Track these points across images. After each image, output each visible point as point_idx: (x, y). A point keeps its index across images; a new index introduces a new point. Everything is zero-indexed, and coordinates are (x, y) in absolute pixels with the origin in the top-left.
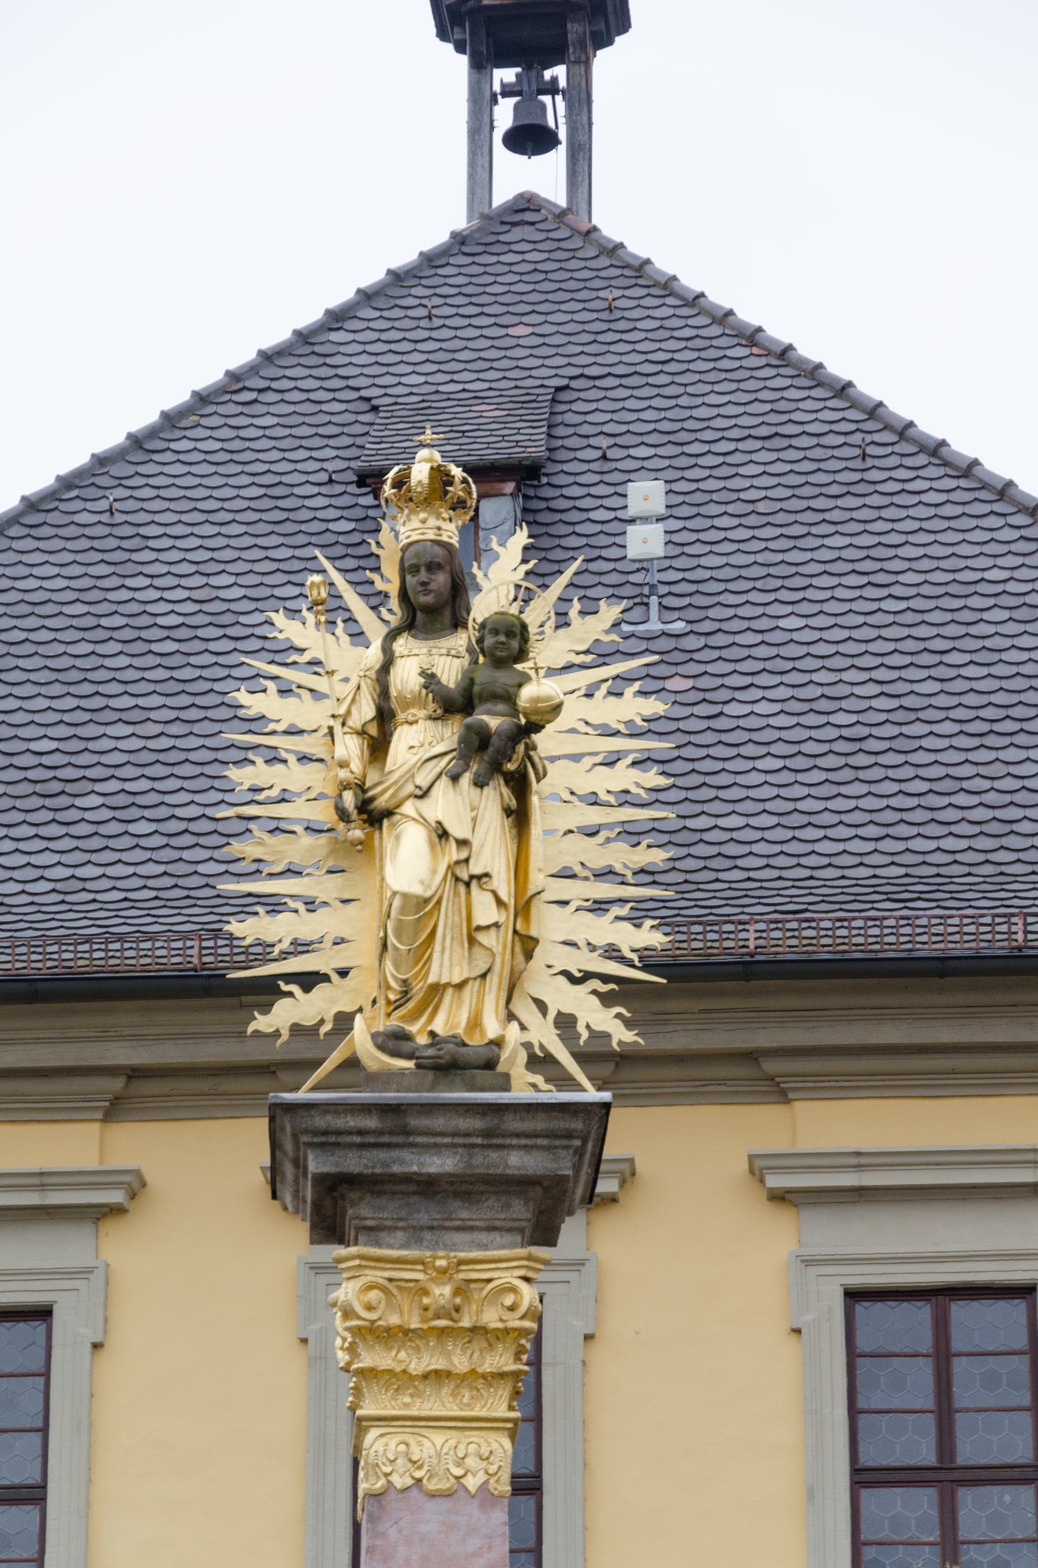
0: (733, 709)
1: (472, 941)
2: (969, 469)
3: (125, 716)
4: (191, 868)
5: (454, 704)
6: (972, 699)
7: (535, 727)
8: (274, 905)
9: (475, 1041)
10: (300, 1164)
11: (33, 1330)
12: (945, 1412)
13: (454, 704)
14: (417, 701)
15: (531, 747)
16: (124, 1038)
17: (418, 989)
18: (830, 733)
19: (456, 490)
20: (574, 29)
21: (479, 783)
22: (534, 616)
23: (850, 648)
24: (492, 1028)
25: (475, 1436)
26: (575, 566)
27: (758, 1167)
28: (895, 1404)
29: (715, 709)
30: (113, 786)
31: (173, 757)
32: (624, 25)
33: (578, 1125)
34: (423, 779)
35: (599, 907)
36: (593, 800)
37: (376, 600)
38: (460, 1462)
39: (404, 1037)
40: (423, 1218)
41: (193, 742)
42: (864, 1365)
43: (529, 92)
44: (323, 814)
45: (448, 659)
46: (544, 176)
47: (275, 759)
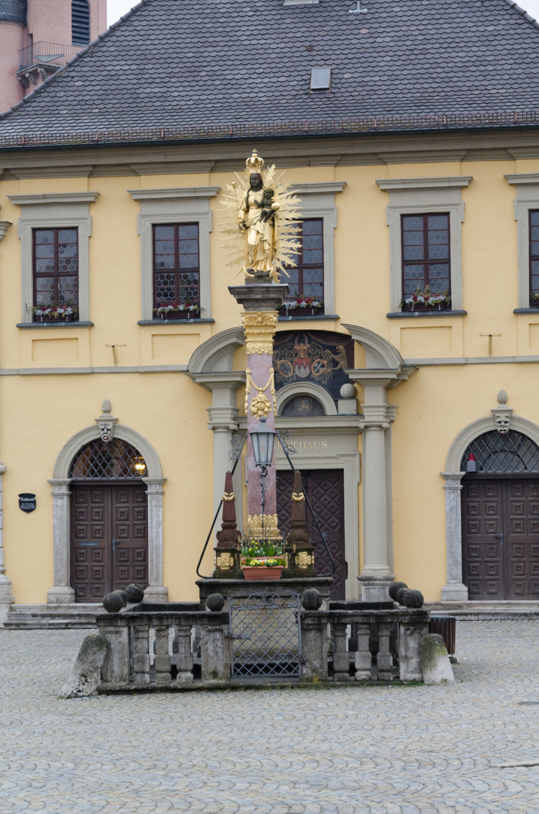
0: (379, 40)
3: (212, 44)
4: (230, 96)
11: (195, 227)
13: (260, 205)
16: (214, 153)
21: (265, 221)
27: (378, 183)
28: (413, 244)
29: (373, 40)
30: (209, 68)
31: (225, 58)
34: (254, 222)
35: (289, 240)
37: (245, 182)
39: (253, 270)
40: (256, 305)
41: (231, 53)
42: (406, 234)
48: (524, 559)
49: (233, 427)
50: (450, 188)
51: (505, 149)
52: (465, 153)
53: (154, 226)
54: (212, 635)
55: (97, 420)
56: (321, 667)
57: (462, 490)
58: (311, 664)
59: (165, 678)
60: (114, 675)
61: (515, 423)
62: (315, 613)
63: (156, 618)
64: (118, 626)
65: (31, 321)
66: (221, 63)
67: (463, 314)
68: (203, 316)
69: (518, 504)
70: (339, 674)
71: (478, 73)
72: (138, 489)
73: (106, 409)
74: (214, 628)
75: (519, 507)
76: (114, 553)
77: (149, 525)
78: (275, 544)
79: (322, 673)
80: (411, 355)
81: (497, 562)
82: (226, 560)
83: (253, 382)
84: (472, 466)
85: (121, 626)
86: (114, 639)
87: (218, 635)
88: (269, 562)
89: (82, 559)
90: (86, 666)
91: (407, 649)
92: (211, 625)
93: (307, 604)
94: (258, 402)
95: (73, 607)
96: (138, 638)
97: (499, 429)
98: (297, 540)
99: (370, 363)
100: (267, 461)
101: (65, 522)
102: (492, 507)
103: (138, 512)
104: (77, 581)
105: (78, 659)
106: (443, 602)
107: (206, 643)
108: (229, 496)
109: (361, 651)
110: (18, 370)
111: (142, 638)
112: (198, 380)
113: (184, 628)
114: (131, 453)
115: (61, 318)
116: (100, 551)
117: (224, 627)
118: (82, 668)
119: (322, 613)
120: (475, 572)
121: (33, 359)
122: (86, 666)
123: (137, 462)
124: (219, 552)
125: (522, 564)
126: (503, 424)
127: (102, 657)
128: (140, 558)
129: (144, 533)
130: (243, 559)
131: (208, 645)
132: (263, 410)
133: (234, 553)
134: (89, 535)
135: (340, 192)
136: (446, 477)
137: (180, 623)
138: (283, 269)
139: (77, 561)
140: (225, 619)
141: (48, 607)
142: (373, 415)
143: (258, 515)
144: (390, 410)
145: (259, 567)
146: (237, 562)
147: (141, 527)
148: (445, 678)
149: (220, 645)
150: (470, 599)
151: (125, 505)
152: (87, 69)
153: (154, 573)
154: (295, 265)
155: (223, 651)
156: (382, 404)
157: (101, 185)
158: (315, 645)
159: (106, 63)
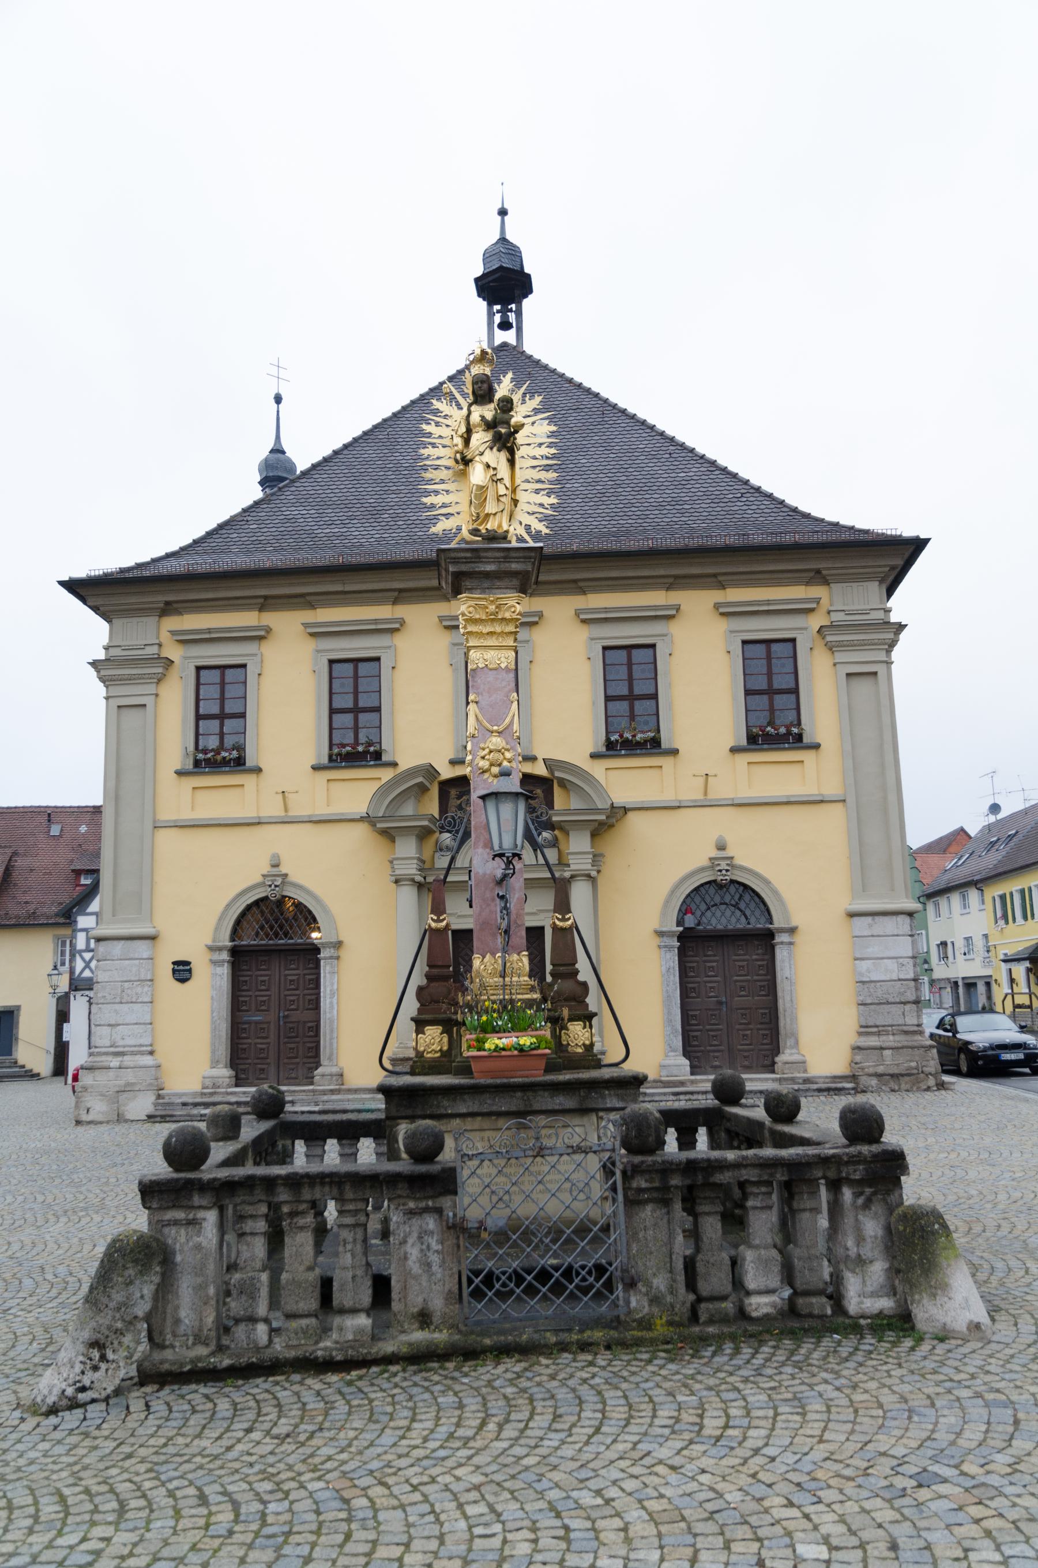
2: (633, 417)
5: (490, 425)
7: (516, 432)
8: (436, 492)
9: (500, 531)
10: (447, 570)
13: (490, 425)
14: (479, 425)
17: (482, 515)
19: (489, 356)
20: (517, 292)
21: (499, 450)
22: (516, 398)
24: (505, 527)
27: (578, 613)
32: (531, 291)
34: (481, 449)
35: (537, 491)
36: (535, 458)
37: (464, 395)
43: (504, 312)
44: (451, 463)
45: (489, 412)
46: (509, 337)
50: (656, 617)
52: (671, 580)
54: (416, 1222)
56: (672, 1291)
58: (649, 1285)
59: (305, 1331)
60: (182, 1329)
61: (736, 872)
64: (193, 1207)
72: (310, 955)
74: (422, 1204)
79: (672, 1306)
80: (620, 796)
84: (690, 921)
85: (200, 1207)
86: (183, 1239)
87: (431, 1222)
88: (522, 1042)
90: (105, 1320)
91: (860, 1239)
92: (415, 1199)
95: (232, 1093)
98: (566, 1000)
99: (575, 803)
105: (87, 1300)
107: (404, 1242)
109: (757, 1247)
111: (252, 1234)
113: (351, 1207)
114: (306, 917)
117: (446, 1202)
118: (93, 1324)
119: (671, 1163)
121: (193, 808)
122: (105, 1320)
123: (314, 930)
124: (420, 1024)
127: (148, 1290)
130: (468, 1037)
131: (408, 1248)
132: (500, 765)
133: (449, 1026)
136: (660, 934)
137: (341, 1193)
139: (239, 1038)
140: (446, 1183)
141: (203, 1094)
142: (579, 863)
143: (493, 954)
145: (503, 1053)
146: (454, 1043)
148: (976, 1320)
149: (435, 1246)
150: (692, 1074)
151: (295, 972)
153: (328, 1051)
154: (547, 531)
155: (443, 1261)
156: (589, 849)
157: (272, 619)
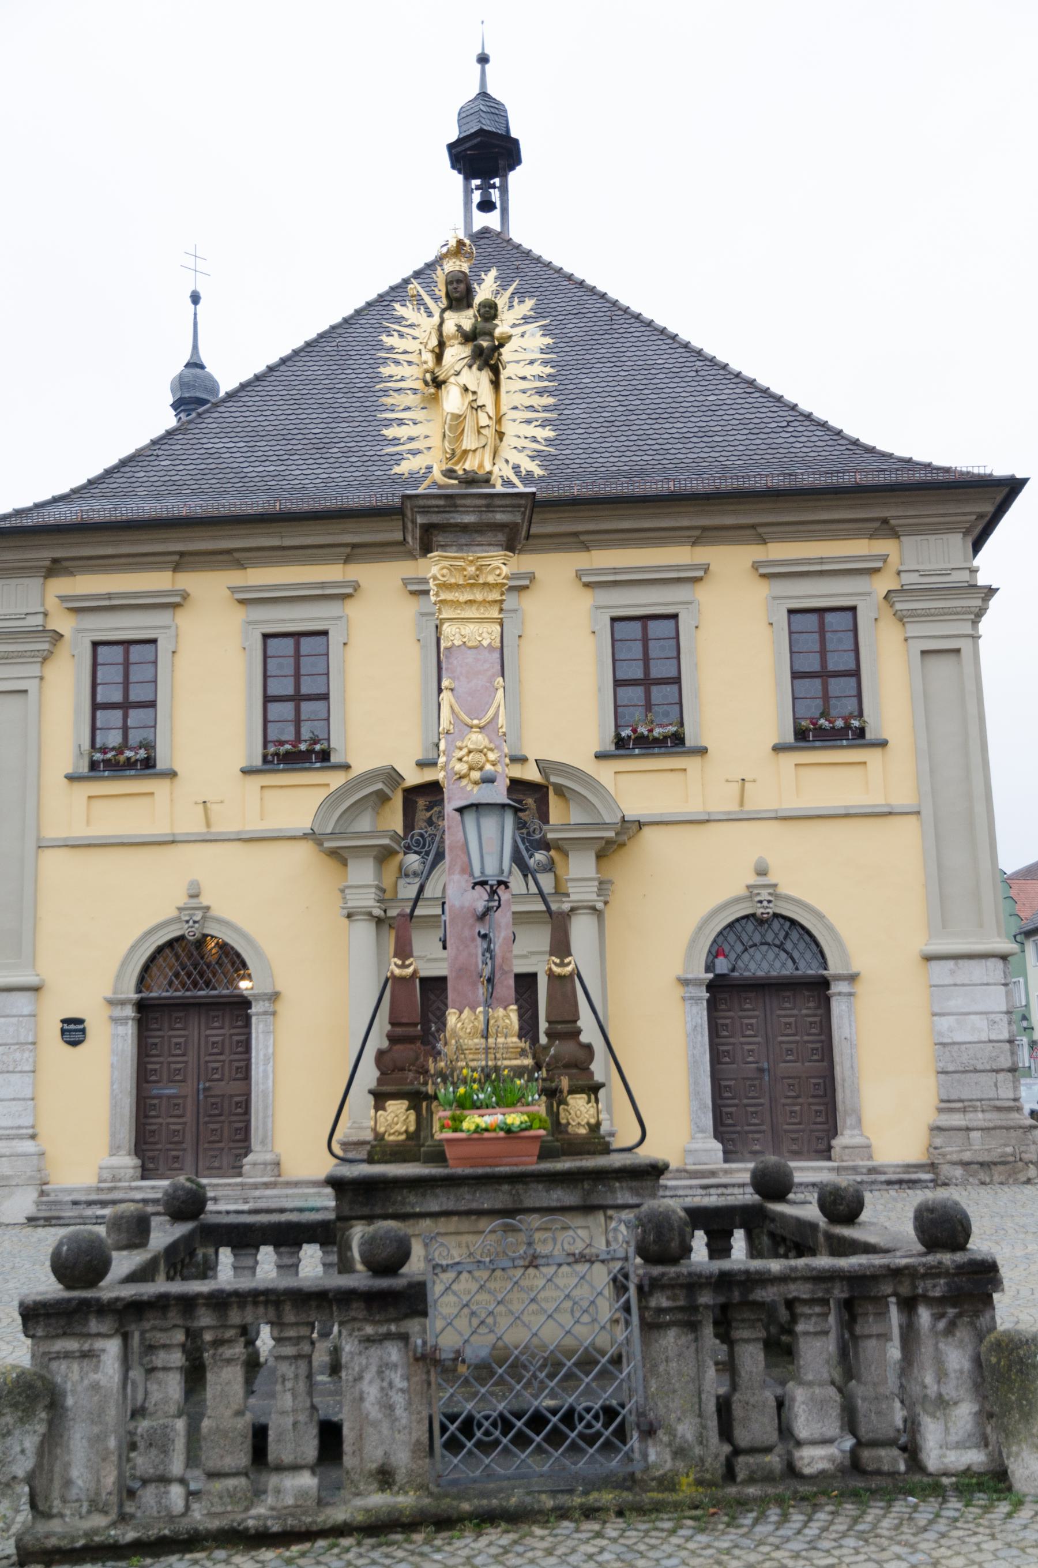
0: (566, 412)
1: (479, 433)
2: (650, 324)
5: (468, 337)
6: (652, 406)
8: (401, 422)
9: (481, 472)
10: (414, 522)
12: (646, 660)
13: (468, 337)
14: (454, 337)
15: (500, 354)
17: (458, 452)
18: (601, 420)
20: (501, 163)
21: (480, 369)
22: (501, 302)
23: (608, 389)
24: (488, 467)
25: (485, 625)
26: (515, 285)
27: (579, 574)
30: (342, 445)
33: (523, 502)
34: (457, 368)
35: (528, 422)
37: (436, 299)
38: (480, 635)
40: (463, 541)
43: (485, 188)
45: (466, 319)
46: (491, 220)
47: (397, 362)
48: (800, 1100)
49: (377, 912)
51: (753, 527)
52: (697, 533)
53: (266, 636)
54: (375, 1353)
55: (180, 909)
56: (701, 1440)
57: (708, 1001)
58: (672, 1432)
59: (231, 1495)
60: (73, 1493)
61: (780, 903)
62: (678, 1275)
63: (207, 1305)
64: (89, 1335)
65: (86, 770)
66: (359, 439)
67: (702, 751)
68: (334, 759)
69: (787, 1020)
70: (751, 1460)
71: (702, 445)
73: (192, 892)
74: (383, 1329)
75: (790, 1024)
76: (202, 1103)
77: (253, 1060)
78: (520, 1076)
79: (702, 1460)
80: (633, 808)
81: (762, 1105)
82: (397, 1118)
83: (457, 708)
84: (722, 966)
85: (99, 1335)
86: (75, 1376)
87: (394, 1353)
89: (153, 1113)
91: (941, 1375)
92: (374, 1323)
93: (654, 1248)
94: (470, 752)
96: (151, 1371)
97: (759, 911)
98: (567, 1066)
99: (576, 816)
100: (502, 871)
101: (129, 1059)
102: (751, 1025)
103: (238, 1042)
104: (145, 1147)
106: (689, 1167)
107: (359, 1378)
108: (403, 966)
109: (810, 1384)
110: (66, 839)
111: (165, 1369)
112: (327, 844)
113: (292, 1333)
114: (233, 962)
115: (130, 764)
116: (180, 1101)
117: (413, 1326)
119: (700, 1275)
120: (730, 1121)
121: (88, 823)
124: (379, 1098)
125: (797, 1108)
126: (765, 904)
127: (30, 1443)
128: (239, 1110)
129: (245, 1073)
130: (441, 1114)
132: (481, 769)
133: (417, 1099)
134: (165, 1077)
135: (527, 587)
136: (685, 982)
137: (279, 1316)
138: (515, 480)
139: (146, 1117)
140: (413, 1301)
142: (581, 893)
143: (473, 1009)
144: (604, 886)
145: (486, 1135)
146: (423, 1123)
147: (242, 1064)
149: (399, 1383)
150: (726, 1161)
151: (219, 1031)
152: (178, 447)
154: (542, 473)
155: (410, 1403)
157: (188, 581)
158: (680, 1373)
159: (204, 441)
